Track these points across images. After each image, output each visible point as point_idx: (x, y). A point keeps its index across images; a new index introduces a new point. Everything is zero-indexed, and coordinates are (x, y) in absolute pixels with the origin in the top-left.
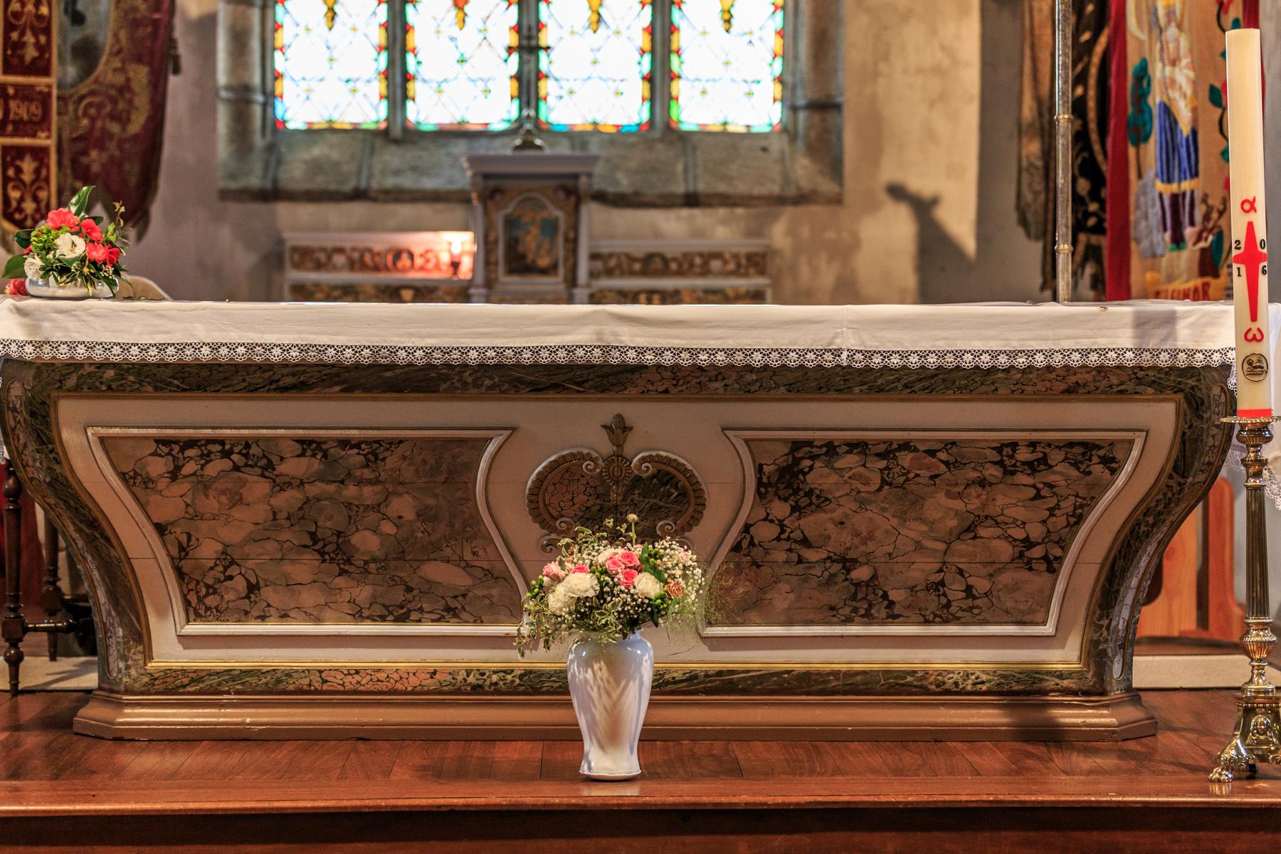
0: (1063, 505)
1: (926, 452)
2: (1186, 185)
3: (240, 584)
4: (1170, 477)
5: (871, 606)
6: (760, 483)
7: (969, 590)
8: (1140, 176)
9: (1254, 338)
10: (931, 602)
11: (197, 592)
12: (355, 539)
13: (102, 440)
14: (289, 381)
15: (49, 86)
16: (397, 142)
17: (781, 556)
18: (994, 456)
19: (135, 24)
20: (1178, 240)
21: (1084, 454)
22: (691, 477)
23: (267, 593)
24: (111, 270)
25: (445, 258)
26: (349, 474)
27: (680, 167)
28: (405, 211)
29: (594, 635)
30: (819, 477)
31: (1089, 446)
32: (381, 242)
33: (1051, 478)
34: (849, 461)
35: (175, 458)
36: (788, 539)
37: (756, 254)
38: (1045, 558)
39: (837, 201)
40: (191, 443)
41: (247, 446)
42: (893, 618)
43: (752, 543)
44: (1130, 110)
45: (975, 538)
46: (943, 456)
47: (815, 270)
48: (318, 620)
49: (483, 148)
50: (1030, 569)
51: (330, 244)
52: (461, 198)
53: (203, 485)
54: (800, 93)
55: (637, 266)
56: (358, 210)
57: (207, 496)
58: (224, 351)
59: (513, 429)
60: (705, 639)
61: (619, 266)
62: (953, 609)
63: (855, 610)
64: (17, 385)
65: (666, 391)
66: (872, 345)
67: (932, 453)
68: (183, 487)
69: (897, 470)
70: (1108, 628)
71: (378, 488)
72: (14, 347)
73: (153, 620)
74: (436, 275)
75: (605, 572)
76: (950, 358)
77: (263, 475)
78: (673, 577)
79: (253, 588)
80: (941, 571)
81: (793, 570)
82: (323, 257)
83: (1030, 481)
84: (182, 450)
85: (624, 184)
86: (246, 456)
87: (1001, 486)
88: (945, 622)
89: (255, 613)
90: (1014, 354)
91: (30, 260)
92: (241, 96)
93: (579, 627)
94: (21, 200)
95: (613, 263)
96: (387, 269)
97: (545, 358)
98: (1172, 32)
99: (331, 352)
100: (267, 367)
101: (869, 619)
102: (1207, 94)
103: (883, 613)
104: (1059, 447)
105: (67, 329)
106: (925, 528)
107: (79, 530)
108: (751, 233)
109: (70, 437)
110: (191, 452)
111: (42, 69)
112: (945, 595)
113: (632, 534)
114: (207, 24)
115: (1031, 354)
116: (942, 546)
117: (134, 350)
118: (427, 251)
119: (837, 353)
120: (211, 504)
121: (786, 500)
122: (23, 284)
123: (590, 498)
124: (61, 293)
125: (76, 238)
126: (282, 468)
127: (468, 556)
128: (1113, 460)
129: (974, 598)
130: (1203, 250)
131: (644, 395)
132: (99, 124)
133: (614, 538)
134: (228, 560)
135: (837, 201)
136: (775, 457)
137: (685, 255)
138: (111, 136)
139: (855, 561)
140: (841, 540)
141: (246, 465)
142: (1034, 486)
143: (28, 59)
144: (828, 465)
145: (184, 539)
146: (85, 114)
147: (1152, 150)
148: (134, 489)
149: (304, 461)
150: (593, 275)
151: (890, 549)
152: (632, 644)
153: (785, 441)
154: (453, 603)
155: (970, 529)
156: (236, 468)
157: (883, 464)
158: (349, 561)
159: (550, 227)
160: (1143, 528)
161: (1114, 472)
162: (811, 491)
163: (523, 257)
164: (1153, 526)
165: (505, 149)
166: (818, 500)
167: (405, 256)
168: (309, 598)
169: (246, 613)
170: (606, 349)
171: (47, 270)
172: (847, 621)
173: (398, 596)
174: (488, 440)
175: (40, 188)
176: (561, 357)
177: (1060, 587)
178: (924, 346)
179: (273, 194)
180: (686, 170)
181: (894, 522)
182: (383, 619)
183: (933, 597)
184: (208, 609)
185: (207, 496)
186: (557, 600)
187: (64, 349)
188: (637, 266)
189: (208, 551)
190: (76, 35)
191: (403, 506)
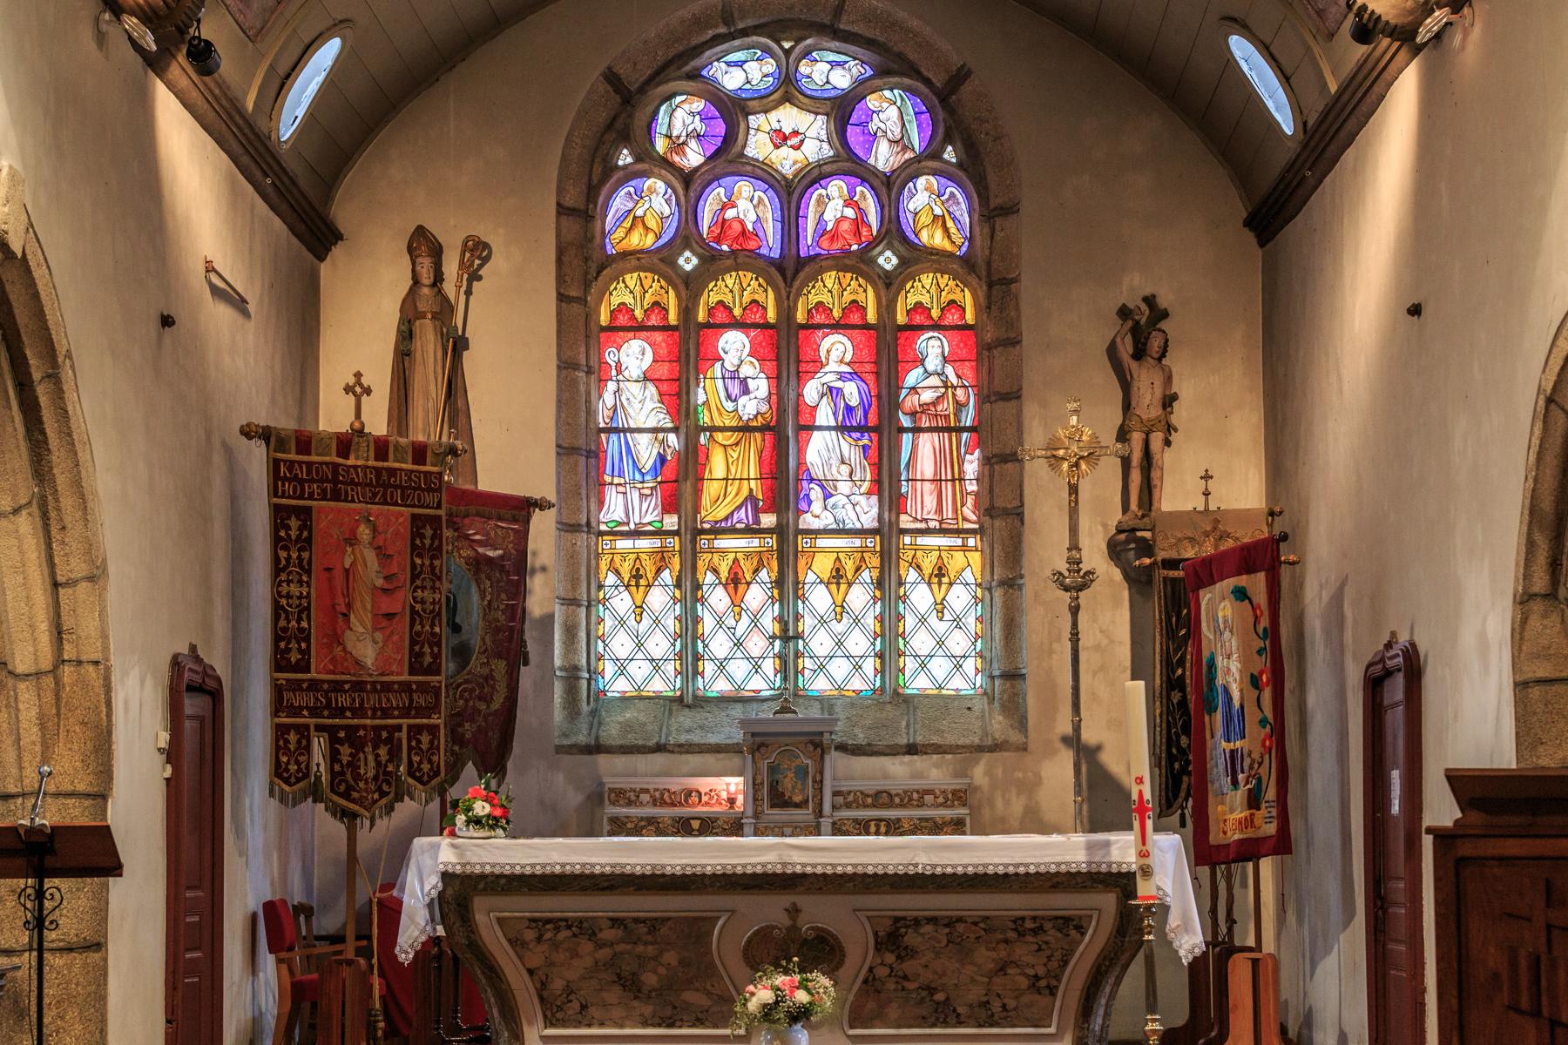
0: (1055, 954)
1: (972, 923)
2: (1238, 744)
3: (576, 1005)
4: (1116, 937)
5: (947, 1016)
6: (876, 943)
7: (1004, 1006)
8: (1212, 737)
9: (1144, 856)
10: (983, 1014)
11: (551, 1010)
12: (643, 978)
13: (499, 920)
14: (605, 884)
15: (440, 682)
16: (688, 706)
17: (891, 986)
18: (1011, 925)
19: (497, 630)
20: (1235, 783)
21: (1064, 924)
22: (836, 939)
23: (593, 1011)
24: (504, 821)
25: (724, 795)
26: (639, 939)
27: (904, 723)
28: (695, 760)
29: (774, 1026)
30: (911, 939)
31: (1067, 919)
32: (676, 784)
33: (1046, 939)
34: (928, 929)
35: (540, 930)
36: (895, 976)
37: (960, 791)
38: (1048, 986)
39: (1024, 748)
40: (549, 921)
41: (581, 922)
42: (960, 1024)
43: (874, 979)
44: (1205, 689)
45: (1005, 974)
46: (982, 925)
47: (1007, 802)
48: (622, 1026)
49: (754, 712)
50: (1040, 994)
51: (638, 787)
52: (734, 749)
53: (556, 946)
54: (995, 665)
55: (869, 800)
56: (659, 760)
57: (557, 952)
58: (568, 867)
59: (733, 912)
60: (849, 1037)
61: (855, 801)
62: (996, 1018)
63: (937, 1019)
64: (450, 888)
65: (821, 889)
66: (935, 861)
67: (975, 924)
68: (544, 947)
69: (956, 934)
70: (1088, 1029)
71: (656, 946)
72: (450, 866)
73: (526, 1029)
74: (717, 809)
75: (779, 989)
76: (981, 868)
77: (589, 940)
78: (818, 993)
79: (584, 1007)
80: (986, 994)
81: (900, 994)
82: (632, 796)
83: (1034, 940)
84: (544, 925)
85: (861, 738)
86: (580, 928)
87: (1018, 943)
88: (991, 1026)
89: (586, 1022)
90: (1017, 865)
91: (459, 816)
92: (572, 674)
93: (765, 1021)
94: (420, 762)
95: (851, 798)
96: (681, 804)
97: (749, 870)
98: (1227, 634)
99: (629, 867)
100: (592, 876)
101: (946, 1024)
102: (1249, 680)
103: (954, 1021)
104: (1049, 920)
105: (480, 856)
106: (976, 969)
107: (484, 973)
108: (956, 775)
109: (480, 918)
110: (548, 926)
111: (434, 669)
112: (990, 1009)
113: (797, 970)
114: (548, 619)
115: (1027, 865)
116: (986, 980)
117: (518, 868)
118: (711, 791)
119: (916, 866)
120: (560, 957)
121: (892, 952)
122: (454, 830)
124: (476, 835)
125: (484, 803)
126: (602, 935)
127: (709, 987)
128: (1082, 927)
129: (1008, 1011)
130: (1250, 790)
131: (808, 891)
132: (471, 703)
133: (786, 972)
134: (569, 990)
135: (1024, 748)
136: (885, 927)
137: (905, 792)
138: (480, 712)
139: (935, 989)
141: (580, 934)
142: (1037, 943)
143: (426, 664)
144: (916, 931)
145: (544, 978)
146: (461, 697)
147: (1219, 716)
148: (517, 949)
149: (613, 931)
150: (834, 807)
151: (956, 981)
152: (795, 1031)
153: (890, 917)
154: (700, 1015)
155: (1002, 969)
156: (575, 935)
157: (947, 930)
158: (639, 991)
159: (802, 772)
160: (1103, 968)
161: (1083, 934)
162: (907, 947)
163: (783, 794)
164: (1109, 966)
165: (767, 712)
167: (694, 794)
168: (617, 1013)
169: (580, 1022)
170: (784, 865)
171: (468, 822)
172: (933, 1025)
173: (668, 1012)
174: (719, 918)
175: (433, 754)
176: (759, 870)
177: (1058, 1004)
178: (966, 861)
179: (596, 749)
180: (908, 726)
181: (957, 965)
182: (660, 1025)
183: (983, 1010)
184: (557, 1020)
185: (557, 952)
186: (753, 1005)
187: (478, 867)
188: (869, 800)
189: (557, 985)
190: (455, 641)
191: (671, 958)
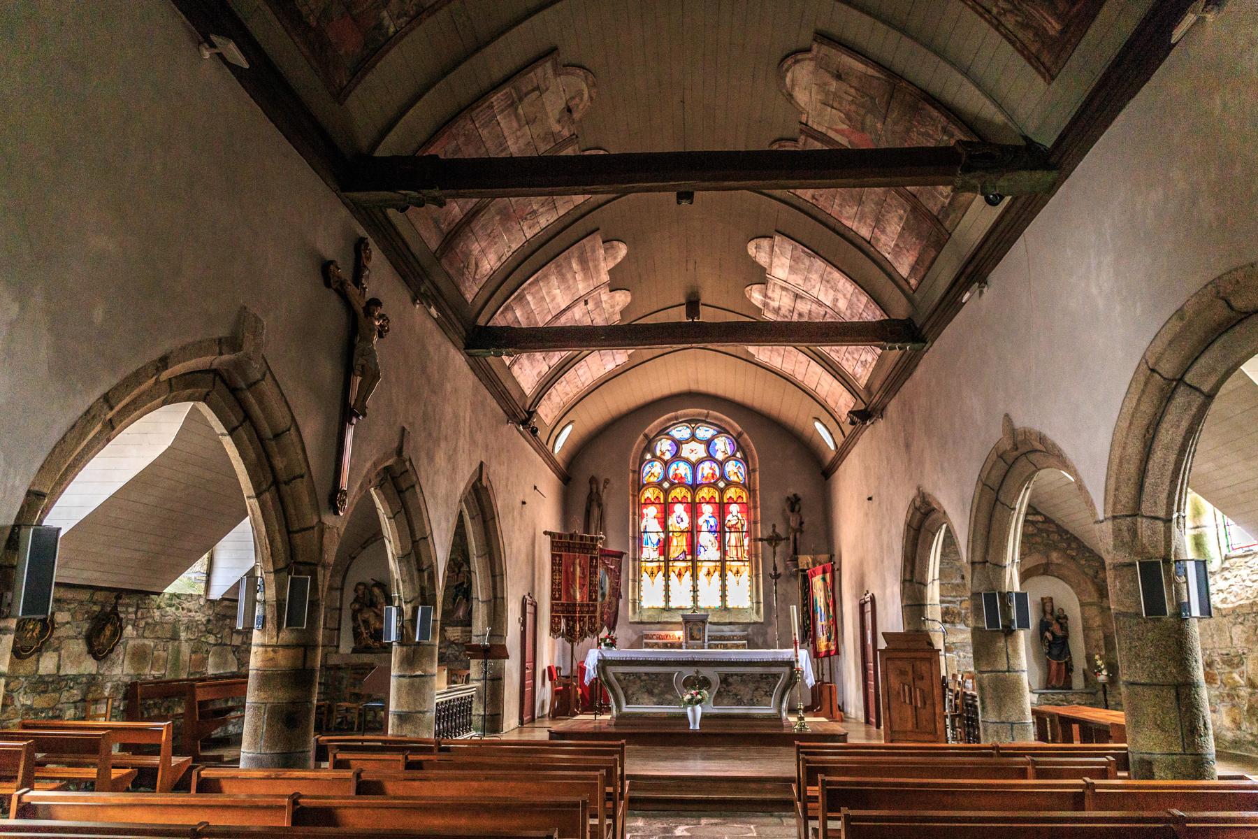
28: (670, 626)
30: (730, 680)
32: (663, 633)
34: (735, 677)
56: (659, 626)
120: (630, 684)
123: (163, 605)
140: (735, 691)
150: (709, 640)
165: (689, 613)
166: (730, 684)
191: (662, 685)
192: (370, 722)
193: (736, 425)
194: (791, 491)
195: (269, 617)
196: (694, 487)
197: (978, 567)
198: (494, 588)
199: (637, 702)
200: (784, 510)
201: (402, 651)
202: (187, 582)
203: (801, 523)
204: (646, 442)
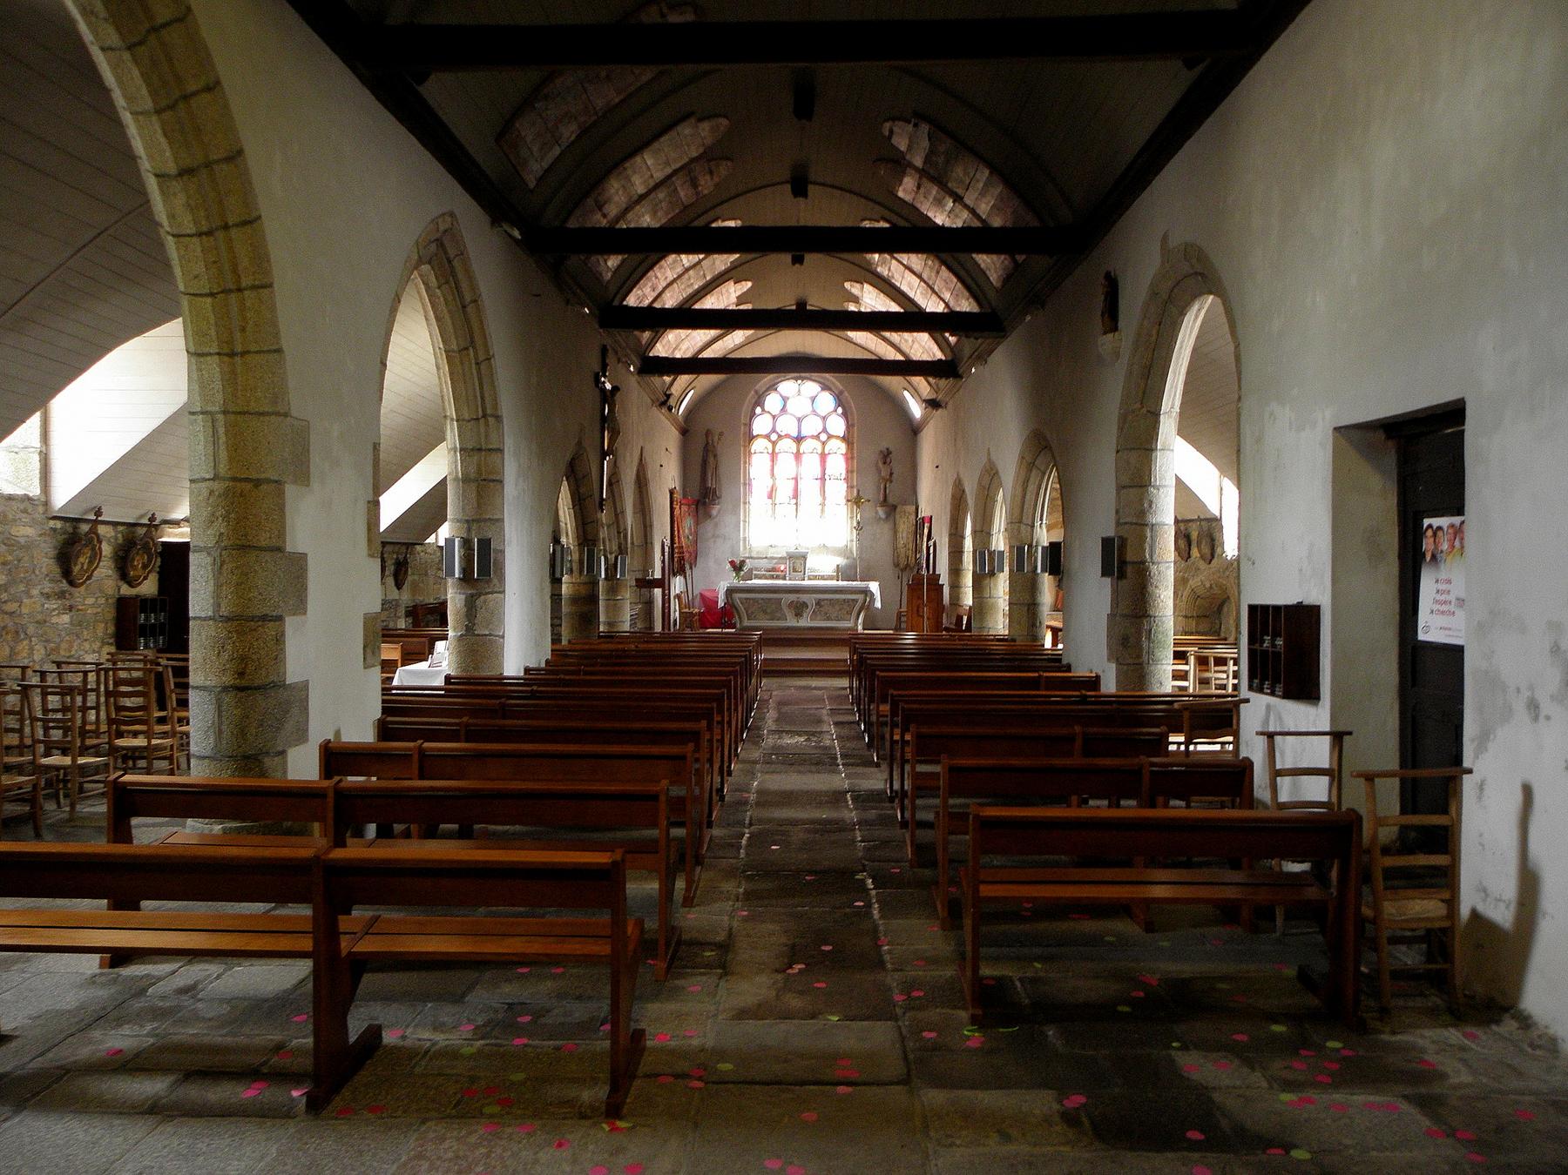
30: (822, 603)
192: (22, 738)
193: (838, 384)
194: (884, 445)
195: (574, 568)
196: (799, 439)
197: (978, 534)
198: (646, 536)
199: (755, 618)
200: (877, 463)
201: (608, 585)
202: (431, 540)
203: (891, 474)
204: (756, 397)
